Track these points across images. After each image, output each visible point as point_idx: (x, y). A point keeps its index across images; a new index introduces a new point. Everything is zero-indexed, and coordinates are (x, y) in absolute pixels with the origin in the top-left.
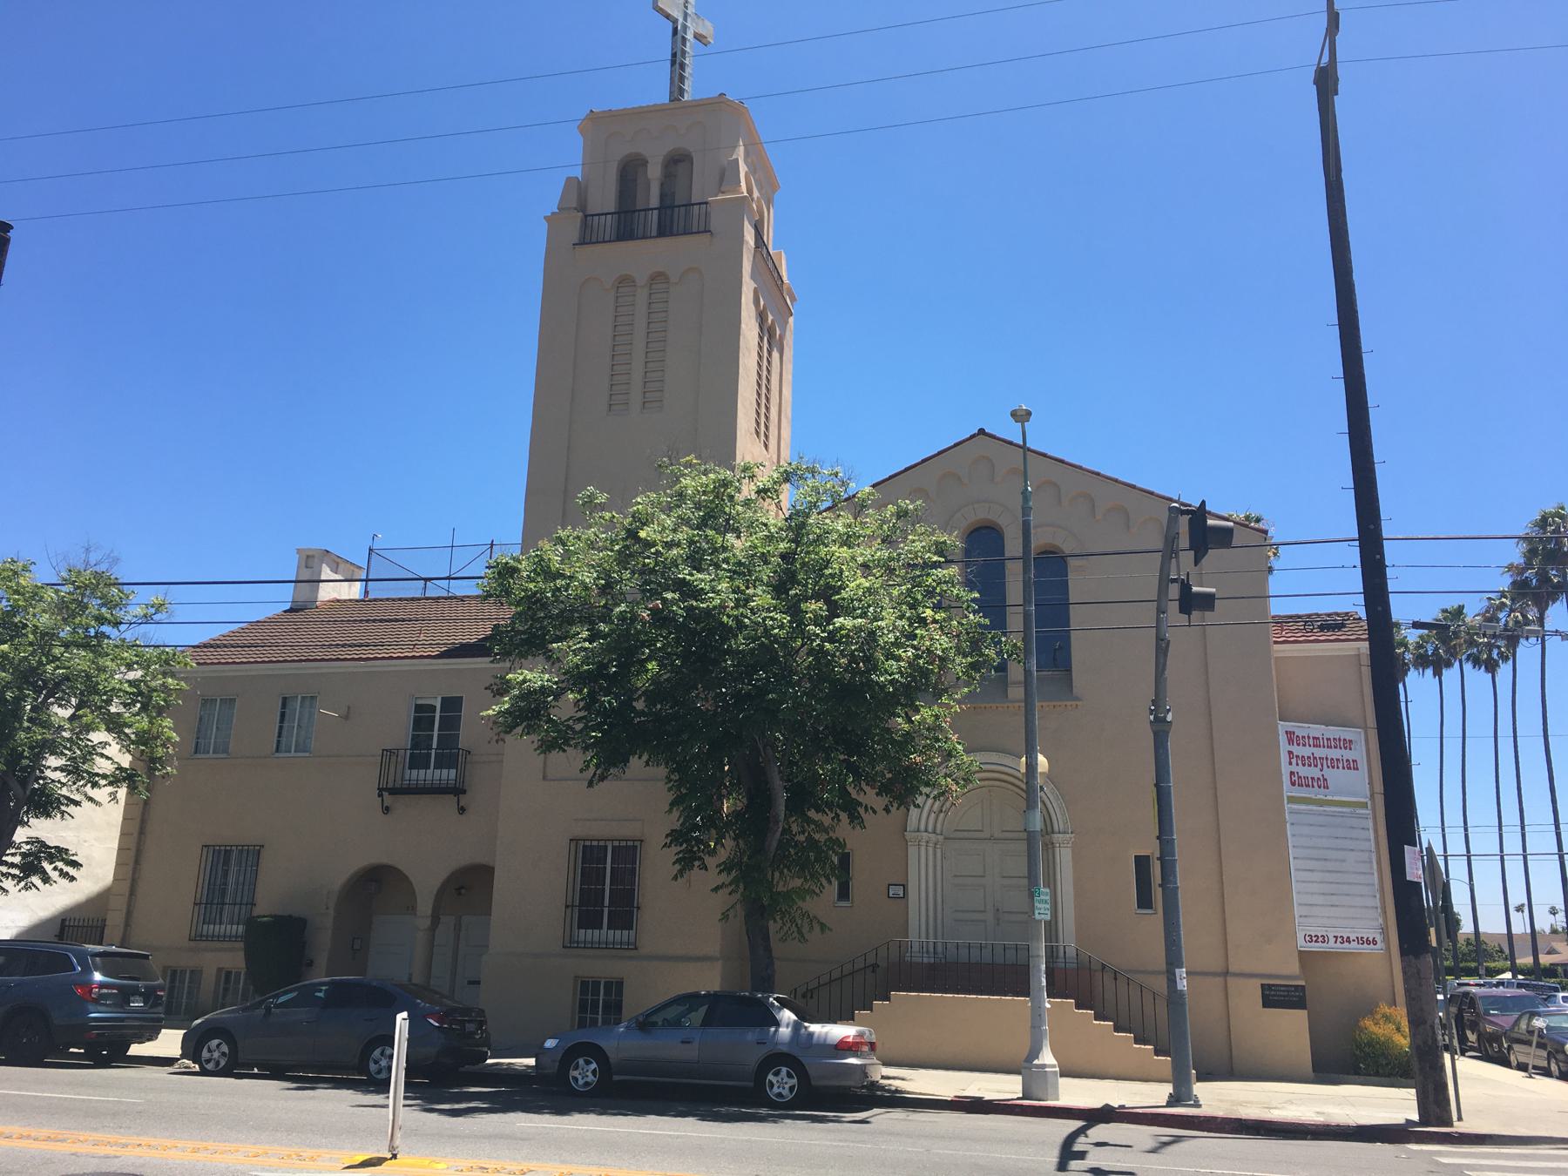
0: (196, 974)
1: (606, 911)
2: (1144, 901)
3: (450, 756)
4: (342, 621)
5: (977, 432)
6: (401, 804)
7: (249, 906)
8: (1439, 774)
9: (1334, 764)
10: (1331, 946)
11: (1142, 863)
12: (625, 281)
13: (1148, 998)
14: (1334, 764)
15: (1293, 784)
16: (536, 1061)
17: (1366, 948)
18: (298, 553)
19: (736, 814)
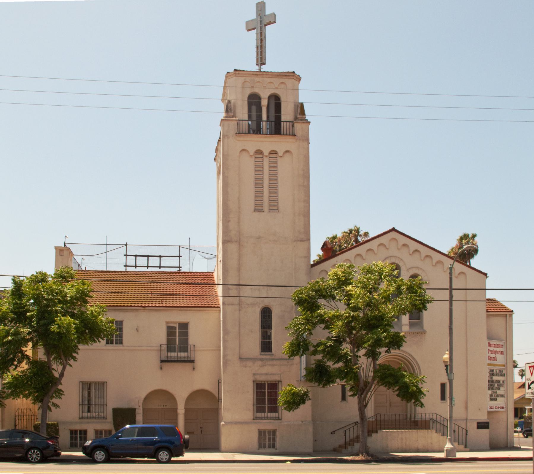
0: (84, 433)
1: (267, 406)
2: (443, 398)
3: (184, 347)
4: (146, 293)
5: (216, 153)
6: (165, 365)
7: (84, 404)
8: (147, 261)
9: (498, 352)
10: (495, 409)
11: (443, 386)
12: (259, 152)
13: (460, 428)
14: (498, 352)
15: (489, 360)
16: (171, 459)
17: (502, 410)
18: (55, 249)
19: (77, 341)
